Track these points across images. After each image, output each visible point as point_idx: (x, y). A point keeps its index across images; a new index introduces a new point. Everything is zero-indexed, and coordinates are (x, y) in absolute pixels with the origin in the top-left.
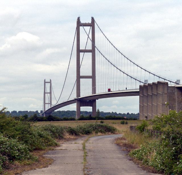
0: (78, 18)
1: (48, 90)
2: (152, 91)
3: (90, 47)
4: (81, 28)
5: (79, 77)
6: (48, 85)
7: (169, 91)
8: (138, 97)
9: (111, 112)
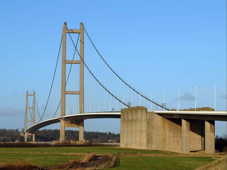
2: (132, 116)
6: (31, 99)
7: (148, 117)
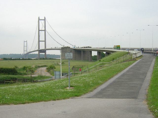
4: (40, 21)
5: (39, 41)
6: (42, 22)
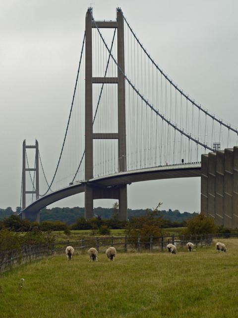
0: (88, 10)
1: (31, 164)
3: (113, 73)
4: (94, 31)
6: (31, 153)
8: (198, 179)
9: (167, 210)
